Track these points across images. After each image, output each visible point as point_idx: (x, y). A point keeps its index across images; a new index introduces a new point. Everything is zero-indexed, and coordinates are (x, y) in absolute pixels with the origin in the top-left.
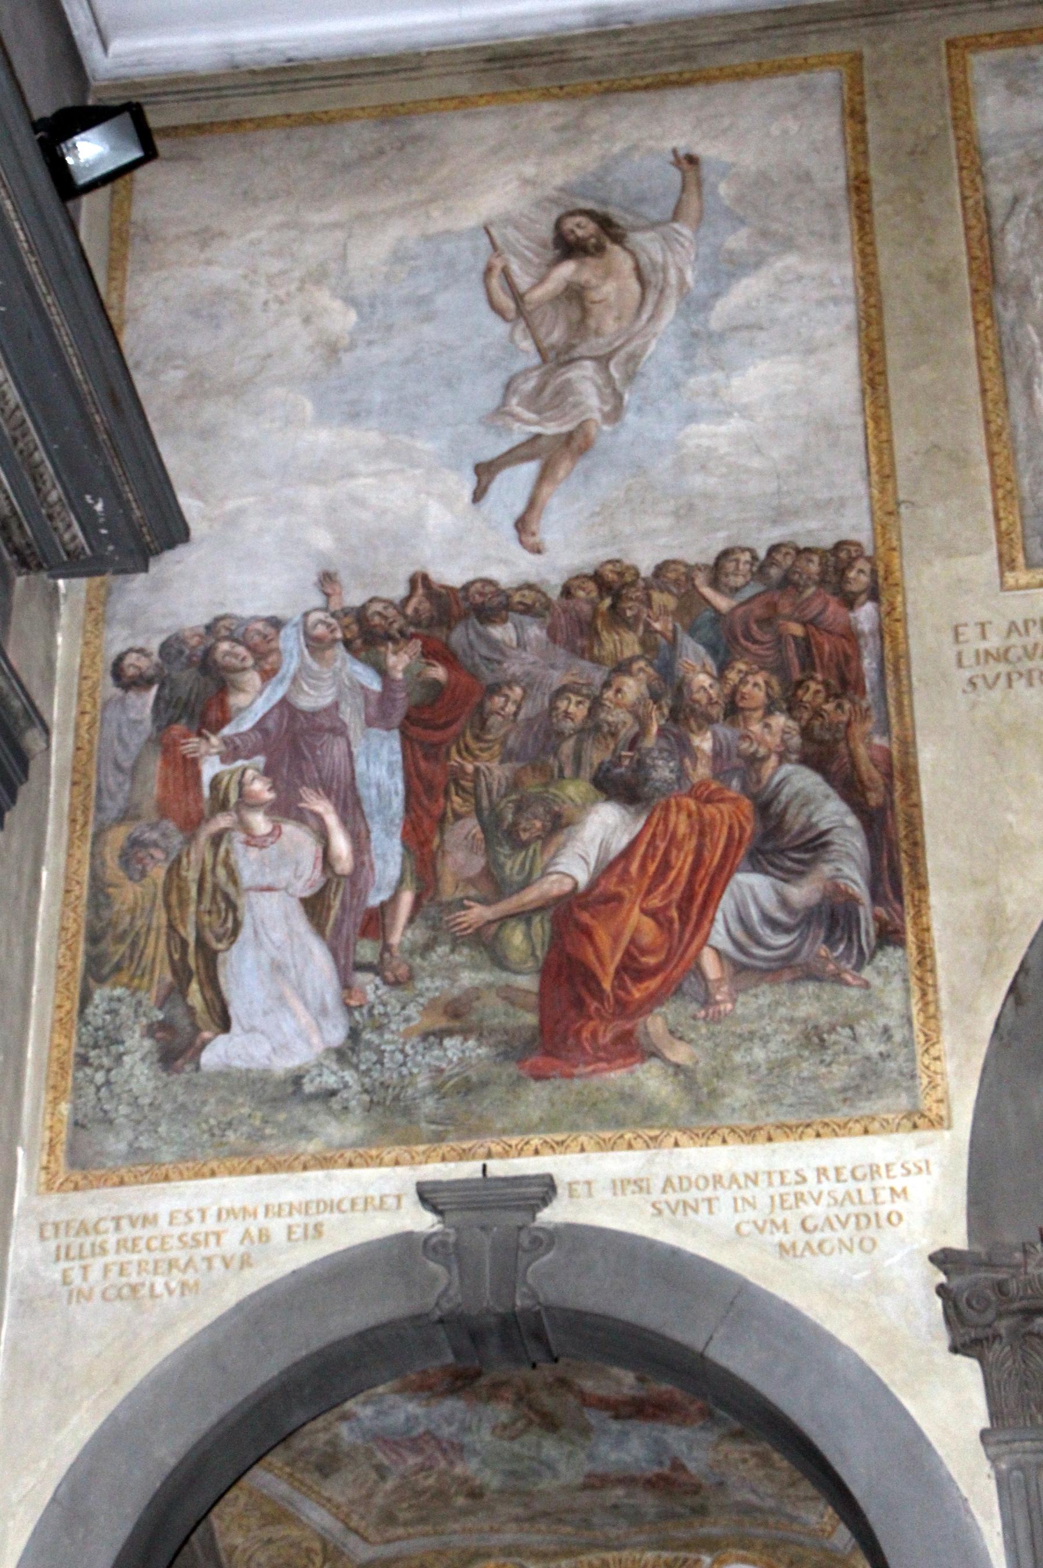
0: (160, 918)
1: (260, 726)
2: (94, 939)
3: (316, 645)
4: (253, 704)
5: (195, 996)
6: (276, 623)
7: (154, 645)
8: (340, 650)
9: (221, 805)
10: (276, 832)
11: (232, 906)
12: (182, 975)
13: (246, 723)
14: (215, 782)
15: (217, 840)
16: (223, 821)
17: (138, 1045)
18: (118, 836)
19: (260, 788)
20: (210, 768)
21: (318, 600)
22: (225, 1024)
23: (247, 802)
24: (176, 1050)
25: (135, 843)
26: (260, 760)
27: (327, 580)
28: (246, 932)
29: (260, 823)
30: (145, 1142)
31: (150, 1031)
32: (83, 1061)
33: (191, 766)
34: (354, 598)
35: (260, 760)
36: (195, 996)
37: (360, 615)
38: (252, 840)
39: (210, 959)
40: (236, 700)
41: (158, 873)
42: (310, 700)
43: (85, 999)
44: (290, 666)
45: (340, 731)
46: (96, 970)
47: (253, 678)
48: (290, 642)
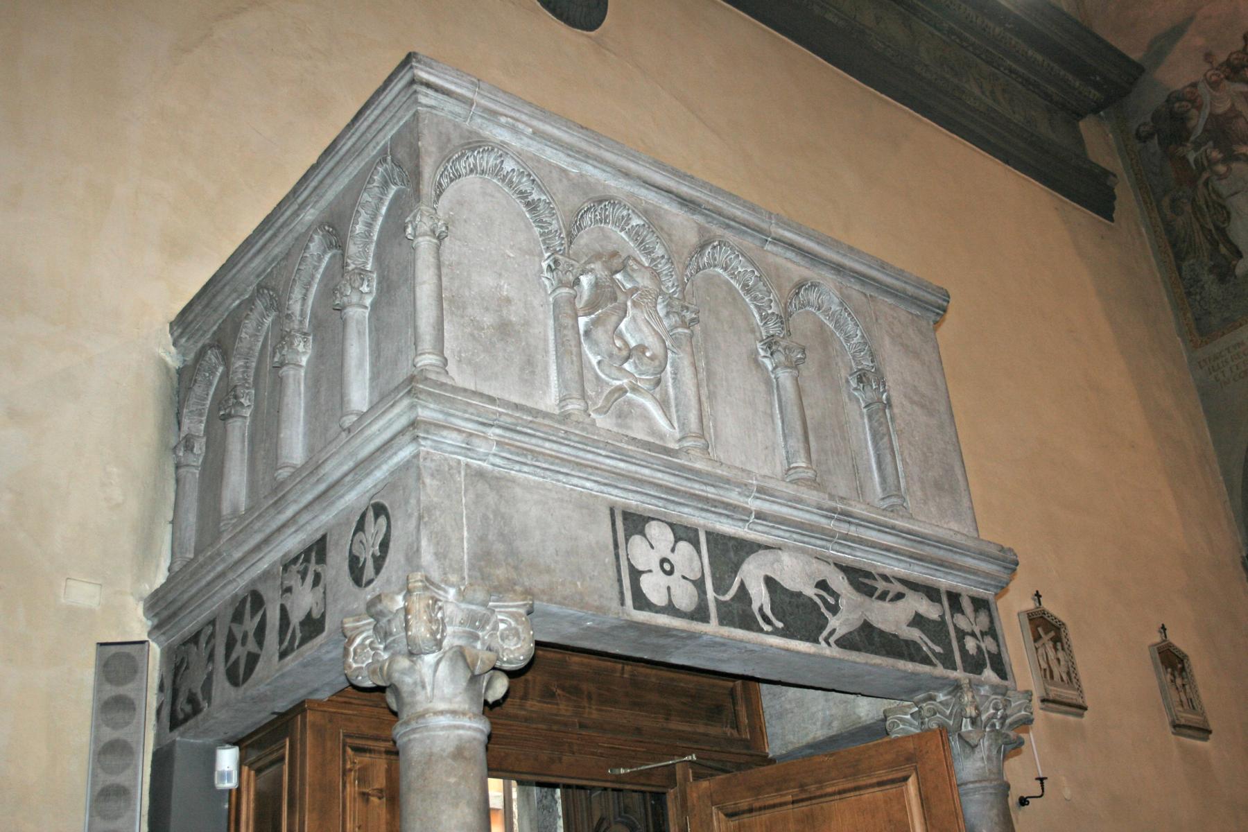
0: (1196, 226)
1: (1205, 130)
2: (1173, 245)
3: (1214, 85)
4: (1198, 122)
5: (1223, 250)
6: (1194, 85)
7: (1149, 119)
8: (1226, 82)
9: (1201, 168)
10: (1229, 169)
11: (1224, 207)
12: (1214, 244)
13: (1199, 131)
14: (1196, 161)
15: (1206, 184)
16: (1205, 175)
17: (1208, 279)
18: (1166, 201)
19: (1216, 155)
20: (1191, 157)
21: (1208, 67)
22: (1239, 254)
23: (1212, 163)
24: (1224, 273)
25: (1173, 200)
26: (1211, 143)
27: (1208, 57)
28: (1234, 215)
29: (1221, 168)
30: (1227, 315)
31: (1211, 271)
32: (1189, 294)
33: (1184, 159)
34: (1222, 58)
35: (1211, 143)
36: (1223, 250)
37: (1228, 63)
38: (1221, 177)
39: (1222, 232)
40: (1191, 124)
41: (1188, 208)
42: (1222, 108)
43: (1179, 269)
44: (1207, 99)
45: (1239, 115)
46: (1179, 257)
47: (1194, 112)
48: (1203, 89)
